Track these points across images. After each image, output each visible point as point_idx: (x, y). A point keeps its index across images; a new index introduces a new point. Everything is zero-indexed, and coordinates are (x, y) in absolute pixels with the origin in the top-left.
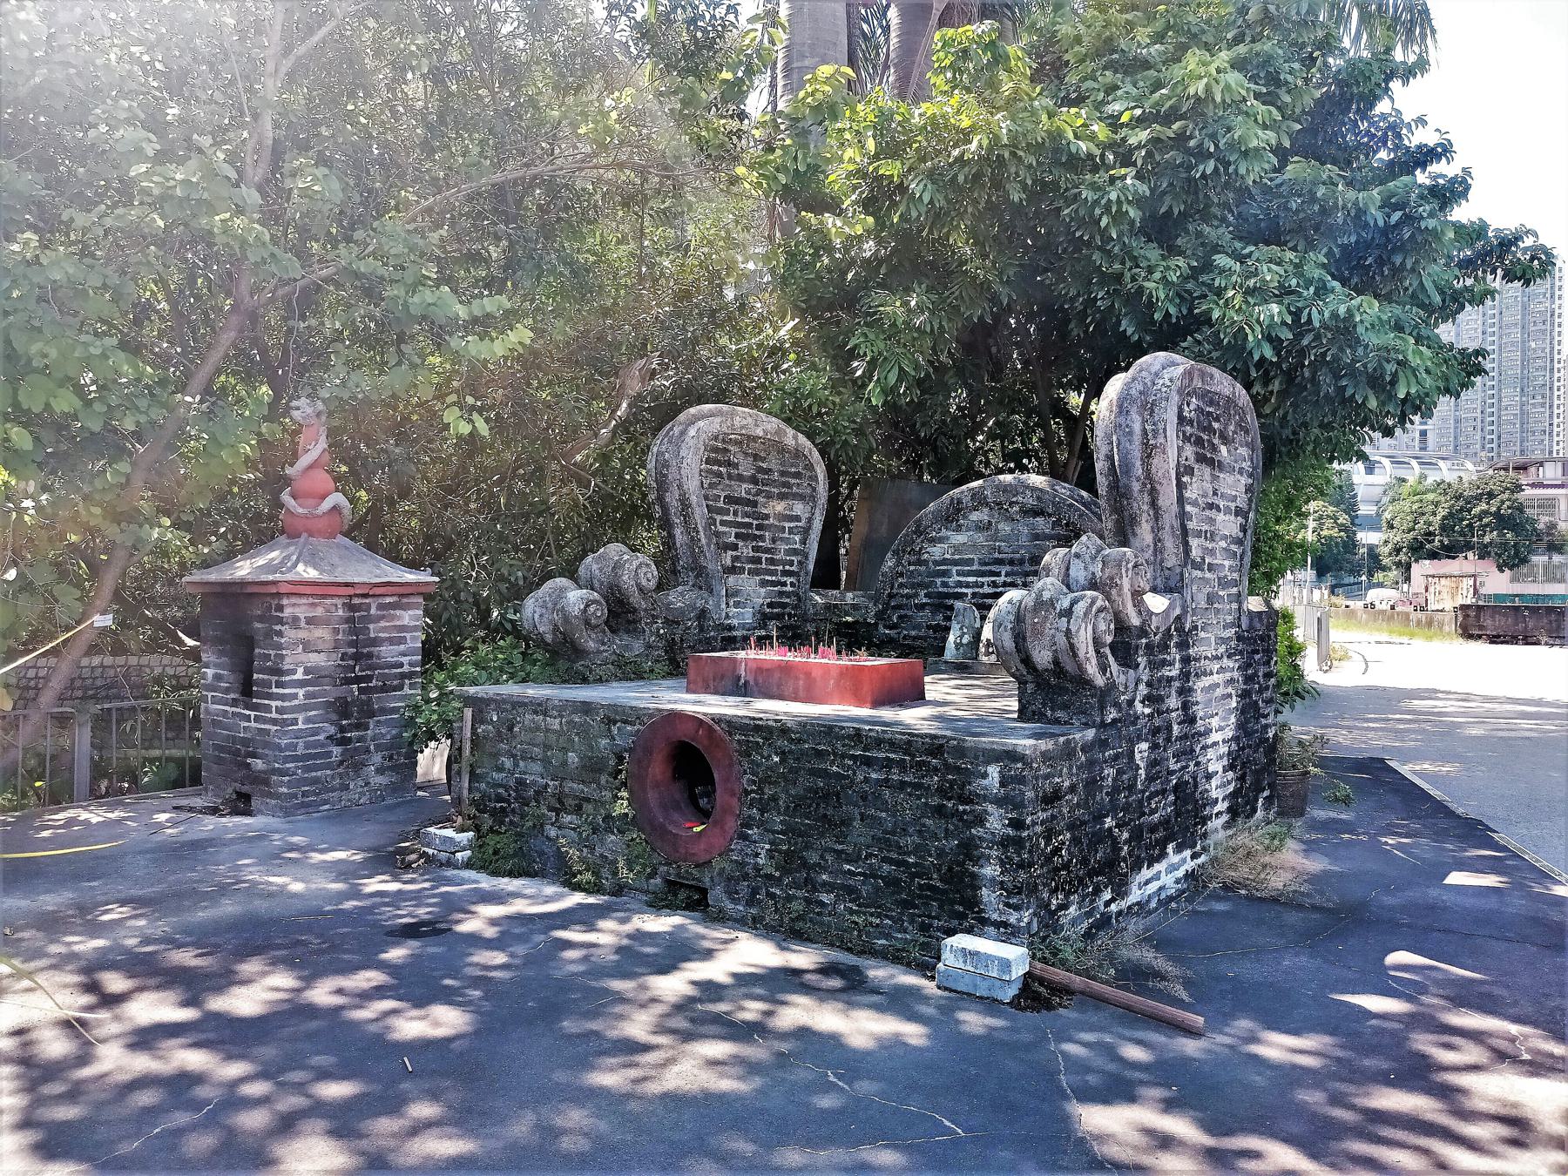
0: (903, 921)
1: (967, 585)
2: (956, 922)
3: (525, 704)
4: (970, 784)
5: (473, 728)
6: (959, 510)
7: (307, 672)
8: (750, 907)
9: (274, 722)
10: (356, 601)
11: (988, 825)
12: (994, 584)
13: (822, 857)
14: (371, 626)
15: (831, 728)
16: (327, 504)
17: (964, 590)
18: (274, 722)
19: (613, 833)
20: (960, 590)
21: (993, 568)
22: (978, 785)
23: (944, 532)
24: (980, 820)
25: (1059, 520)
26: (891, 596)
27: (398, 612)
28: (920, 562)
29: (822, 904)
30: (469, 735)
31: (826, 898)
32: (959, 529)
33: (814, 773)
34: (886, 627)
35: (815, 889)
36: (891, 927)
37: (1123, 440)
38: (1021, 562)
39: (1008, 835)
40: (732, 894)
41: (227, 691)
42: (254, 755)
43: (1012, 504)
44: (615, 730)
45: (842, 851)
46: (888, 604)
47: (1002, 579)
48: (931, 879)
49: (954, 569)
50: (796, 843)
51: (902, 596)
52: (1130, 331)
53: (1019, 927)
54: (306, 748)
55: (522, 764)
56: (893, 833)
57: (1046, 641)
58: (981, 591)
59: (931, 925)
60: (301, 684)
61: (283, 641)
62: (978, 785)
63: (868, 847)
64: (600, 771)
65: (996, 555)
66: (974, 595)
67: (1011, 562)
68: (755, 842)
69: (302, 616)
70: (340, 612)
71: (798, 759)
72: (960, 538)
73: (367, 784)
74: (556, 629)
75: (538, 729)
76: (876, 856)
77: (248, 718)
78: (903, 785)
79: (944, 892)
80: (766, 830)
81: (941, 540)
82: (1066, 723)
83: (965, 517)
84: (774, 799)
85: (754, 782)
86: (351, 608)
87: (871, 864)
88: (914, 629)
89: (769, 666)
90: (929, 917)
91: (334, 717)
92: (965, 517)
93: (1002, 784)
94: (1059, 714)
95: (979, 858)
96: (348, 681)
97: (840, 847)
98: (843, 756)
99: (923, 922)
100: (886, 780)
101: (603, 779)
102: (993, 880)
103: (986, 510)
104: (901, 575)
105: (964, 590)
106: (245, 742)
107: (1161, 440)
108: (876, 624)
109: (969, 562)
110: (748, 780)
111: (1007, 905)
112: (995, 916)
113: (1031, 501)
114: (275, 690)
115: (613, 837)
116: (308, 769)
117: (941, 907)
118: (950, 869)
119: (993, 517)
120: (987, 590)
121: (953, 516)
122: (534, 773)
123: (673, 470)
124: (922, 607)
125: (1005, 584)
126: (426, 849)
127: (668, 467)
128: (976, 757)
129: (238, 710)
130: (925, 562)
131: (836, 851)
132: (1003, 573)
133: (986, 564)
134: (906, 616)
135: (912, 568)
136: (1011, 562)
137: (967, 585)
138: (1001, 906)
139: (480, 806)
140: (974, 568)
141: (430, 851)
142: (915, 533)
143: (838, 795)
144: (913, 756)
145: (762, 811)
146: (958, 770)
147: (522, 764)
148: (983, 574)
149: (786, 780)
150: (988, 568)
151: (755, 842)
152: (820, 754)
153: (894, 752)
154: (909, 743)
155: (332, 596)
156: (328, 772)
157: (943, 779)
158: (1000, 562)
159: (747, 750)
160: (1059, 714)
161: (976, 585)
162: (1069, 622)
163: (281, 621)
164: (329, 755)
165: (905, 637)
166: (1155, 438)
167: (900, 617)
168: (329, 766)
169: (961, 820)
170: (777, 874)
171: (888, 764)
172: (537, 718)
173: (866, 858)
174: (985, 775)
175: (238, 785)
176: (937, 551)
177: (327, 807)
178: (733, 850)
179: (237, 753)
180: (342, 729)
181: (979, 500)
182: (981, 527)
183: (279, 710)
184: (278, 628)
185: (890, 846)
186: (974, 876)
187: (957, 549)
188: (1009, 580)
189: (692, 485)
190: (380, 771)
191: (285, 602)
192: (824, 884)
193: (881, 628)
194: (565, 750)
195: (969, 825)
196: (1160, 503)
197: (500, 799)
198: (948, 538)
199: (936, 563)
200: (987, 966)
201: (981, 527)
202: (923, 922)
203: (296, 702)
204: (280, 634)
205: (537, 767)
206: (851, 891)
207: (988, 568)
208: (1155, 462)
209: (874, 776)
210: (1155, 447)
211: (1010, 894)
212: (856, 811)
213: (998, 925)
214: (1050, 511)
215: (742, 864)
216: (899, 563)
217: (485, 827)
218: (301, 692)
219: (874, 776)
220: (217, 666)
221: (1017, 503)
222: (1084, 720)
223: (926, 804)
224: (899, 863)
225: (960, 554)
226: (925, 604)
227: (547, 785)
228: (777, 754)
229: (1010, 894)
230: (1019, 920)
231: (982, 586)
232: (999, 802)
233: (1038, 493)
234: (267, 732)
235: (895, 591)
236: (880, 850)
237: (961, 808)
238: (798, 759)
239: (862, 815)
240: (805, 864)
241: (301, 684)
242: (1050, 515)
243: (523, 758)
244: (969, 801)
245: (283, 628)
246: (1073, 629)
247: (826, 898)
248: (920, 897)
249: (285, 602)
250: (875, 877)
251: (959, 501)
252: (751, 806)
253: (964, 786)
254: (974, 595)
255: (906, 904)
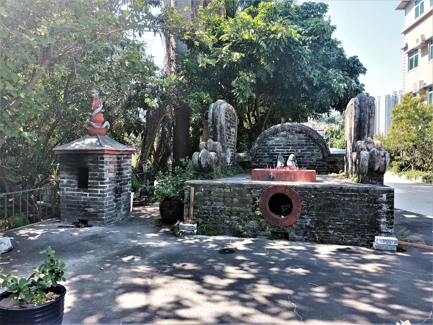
0: (356, 235)
1: (280, 151)
2: (373, 234)
3: (216, 185)
4: (377, 199)
5: (195, 192)
6: (277, 132)
7: (109, 179)
8: (304, 236)
9: (100, 196)
10: (119, 156)
11: (383, 209)
12: (288, 151)
13: (329, 221)
14: (122, 164)
15: (332, 187)
16: (105, 125)
17: (279, 153)
18: (100, 196)
19: (252, 220)
20: (277, 153)
21: (287, 147)
22: (380, 199)
23: (273, 137)
24: (380, 208)
25: (306, 134)
26: (256, 154)
27: (127, 160)
28: (265, 145)
29: (330, 233)
30: (193, 195)
31: (330, 232)
32: (277, 136)
33: (326, 199)
34: (255, 163)
35: (327, 230)
36: (352, 237)
37: (365, 114)
38: (296, 145)
39: (389, 211)
40: (297, 234)
41: (74, 186)
42: (90, 207)
43: (293, 130)
44: (252, 191)
45: (336, 219)
46: (256, 157)
47: (290, 150)
48: (365, 224)
49: (276, 147)
50: (320, 218)
51: (260, 154)
52: (306, 87)
53: (392, 233)
54: (109, 203)
55: (214, 203)
56: (353, 213)
57: (379, 163)
58: (284, 153)
59: (365, 235)
60: (108, 183)
61: (104, 169)
62: (380, 199)
63: (345, 217)
64: (247, 203)
65: (288, 143)
66: (282, 154)
67: (293, 145)
68: (306, 219)
69: (108, 161)
70: (116, 160)
71: (321, 196)
72: (278, 139)
73: (121, 214)
74: (207, 163)
75: (221, 192)
76: (348, 219)
77: (86, 195)
78: (356, 201)
79: (369, 226)
80: (310, 215)
81: (272, 139)
82: (375, 184)
83: (279, 133)
84: (313, 207)
85: (305, 203)
86: (118, 158)
87: (346, 222)
88: (263, 163)
89: (281, 172)
90: (364, 233)
91: (115, 193)
92: (279, 133)
93: (387, 198)
94: (373, 181)
95: (380, 217)
96: (118, 182)
97: (335, 218)
98: (336, 194)
99: (362, 235)
100: (351, 200)
101: (248, 205)
102: (384, 222)
103: (285, 132)
104: (260, 149)
105: (279, 153)
106: (84, 203)
107: (373, 115)
108: (252, 162)
109: (280, 145)
110: (303, 203)
111: (388, 228)
112: (385, 231)
113: (298, 130)
114: (99, 185)
115: (252, 221)
116: (109, 210)
117: (368, 230)
118: (371, 221)
119: (287, 133)
120: (285, 152)
121: (275, 133)
122: (220, 205)
123: (219, 118)
124: (266, 157)
125: (291, 151)
126: (182, 230)
127: (218, 117)
128: (379, 192)
129: (81, 193)
130: (267, 145)
131: (334, 219)
132: (290, 148)
133: (285, 146)
134: (261, 160)
135: (263, 147)
136: (293, 145)
137: (280, 151)
138: (386, 228)
139: (197, 216)
140: (282, 147)
141: (184, 231)
142: (264, 137)
143: (335, 205)
144: (359, 193)
145: (308, 211)
146: (374, 196)
147: (214, 203)
148: (284, 148)
149: (317, 202)
150: (286, 147)
151: (306, 219)
152: (328, 194)
153: (353, 192)
154: (358, 190)
155: (114, 154)
156: (113, 211)
157: (369, 198)
158: (290, 145)
159: (302, 195)
160: (373, 181)
161: (282, 151)
162: (385, 158)
163: (103, 163)
164: (113, 205)
165: (261, 165)
166: (372, 114)
167: (259, 160)
168: (113, 209)
169: (375, 208)
170: (314, 227)
171: (351, 196)
172: (220, 189)
173: (344, 220)
174: (382, 197)
175: (80, 218)
176: (270, 142)
177: (113, 222)
178: (297, 222)
179: (80, 207)
180: (116, 197)
181: (283, 129)
182: (284, 136)
183: (101, 192)
184: (101, 165)
185: (352, 216)
186: (379, 222)
187: (277, 142)
188: (292, 150)
189: (223, 122)
190: (124, 210)
191: (104, 156)
192: (330, 228)
193: (253, 163)
194: (232, 198)
195: (377, 209)
196: (370, 130)
197: (205, 213)
198: (274, 139)
199: (270, 145)
200: (391, 243)
201: (284, 136)
202: (362, 235)
203: (107, 189)
204: (103, 167)
205: (221, 203)
206: (339, 230)
207: (286, 147)
208: (371, 120)
209: (347, 199)
210: (371, 116)
211: (389, 225)
212: (341, 209)
213: (385, 233)
214: (304, 132)
215: (300, 225)
216: (259, 145)
217: (200, 222)
218: (108, 185)
219: (347, 199)
220: (68, 178)
221: (295, 130)
222: (380, 183)
223: (364, 205)
224: (354, 221)
225: (277, 143)
226: (267, 156)
227: (225, 208)
228: (313, 195)
229: (389, 225)
230: (392, 231)
231: (284, 151)
232: (386, 203)
233: (301, 128)
234: (97, 199)
235: (257, 153)
236: (349, 218)
237: (374, 205)
238: (321, 196)
239: (342, 209)
240: (324, 224)
241: (108, 183)
242: (304, 133)
243: (214, 201)
244: (378, 203)
245: (104, 165)
246: (386, 160)
247: (330, 232)
248: (361, 228)
249: (104, 156)
250: (347, 225)
251: (277, 129)
252: (304, 210)
253: (376, 200)
254: (282, 154)
255: (357, 231)
